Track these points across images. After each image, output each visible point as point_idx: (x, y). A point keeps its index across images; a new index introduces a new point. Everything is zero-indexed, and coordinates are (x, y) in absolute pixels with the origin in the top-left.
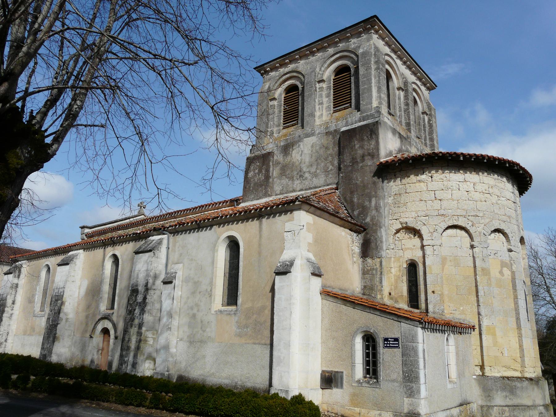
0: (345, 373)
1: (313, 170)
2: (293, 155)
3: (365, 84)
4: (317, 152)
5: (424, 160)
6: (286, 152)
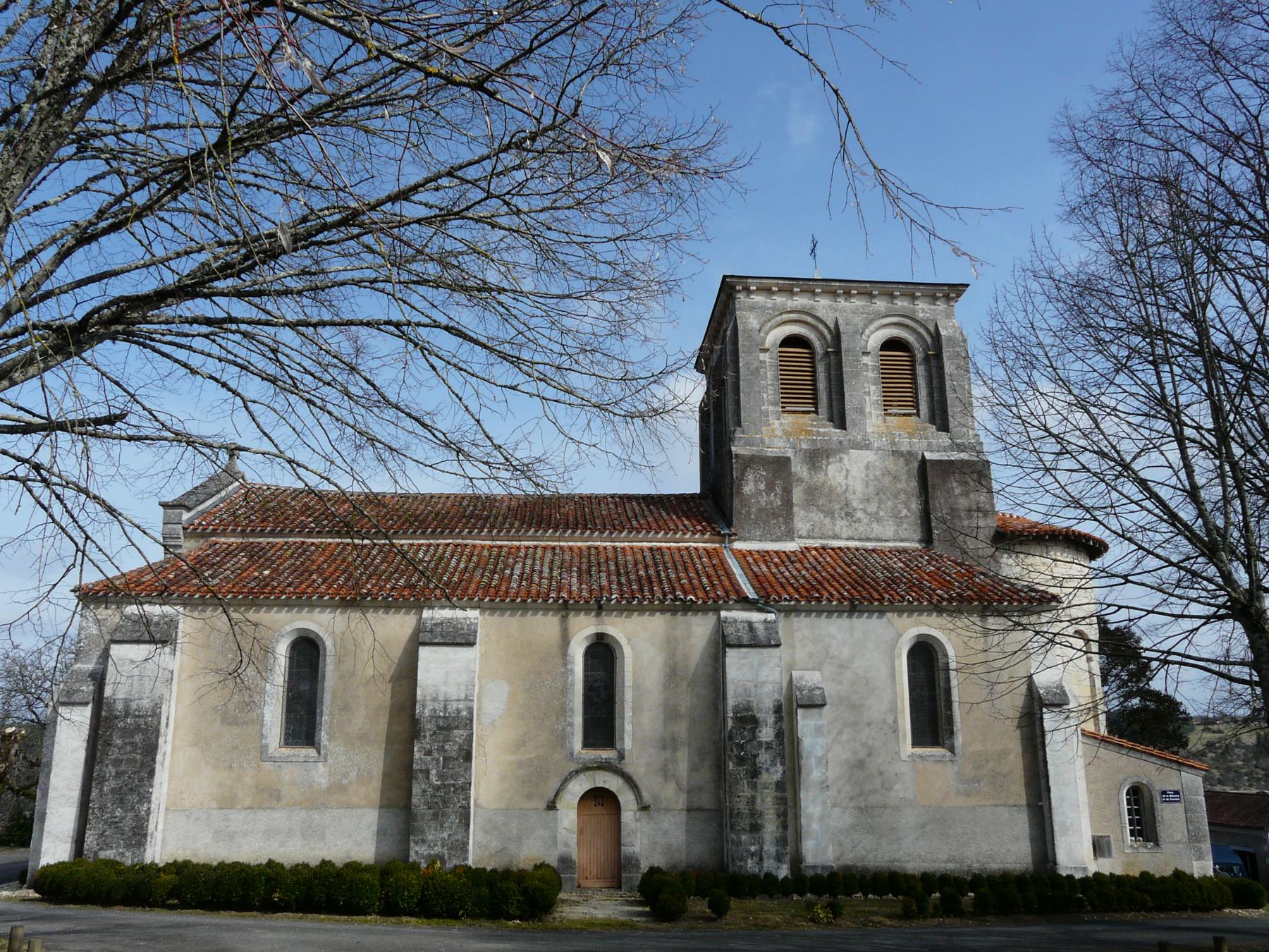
0: (1112, 837)
1: (872, 508)
2: (830, 473)
4: (877, 479)
6: (814, 464)
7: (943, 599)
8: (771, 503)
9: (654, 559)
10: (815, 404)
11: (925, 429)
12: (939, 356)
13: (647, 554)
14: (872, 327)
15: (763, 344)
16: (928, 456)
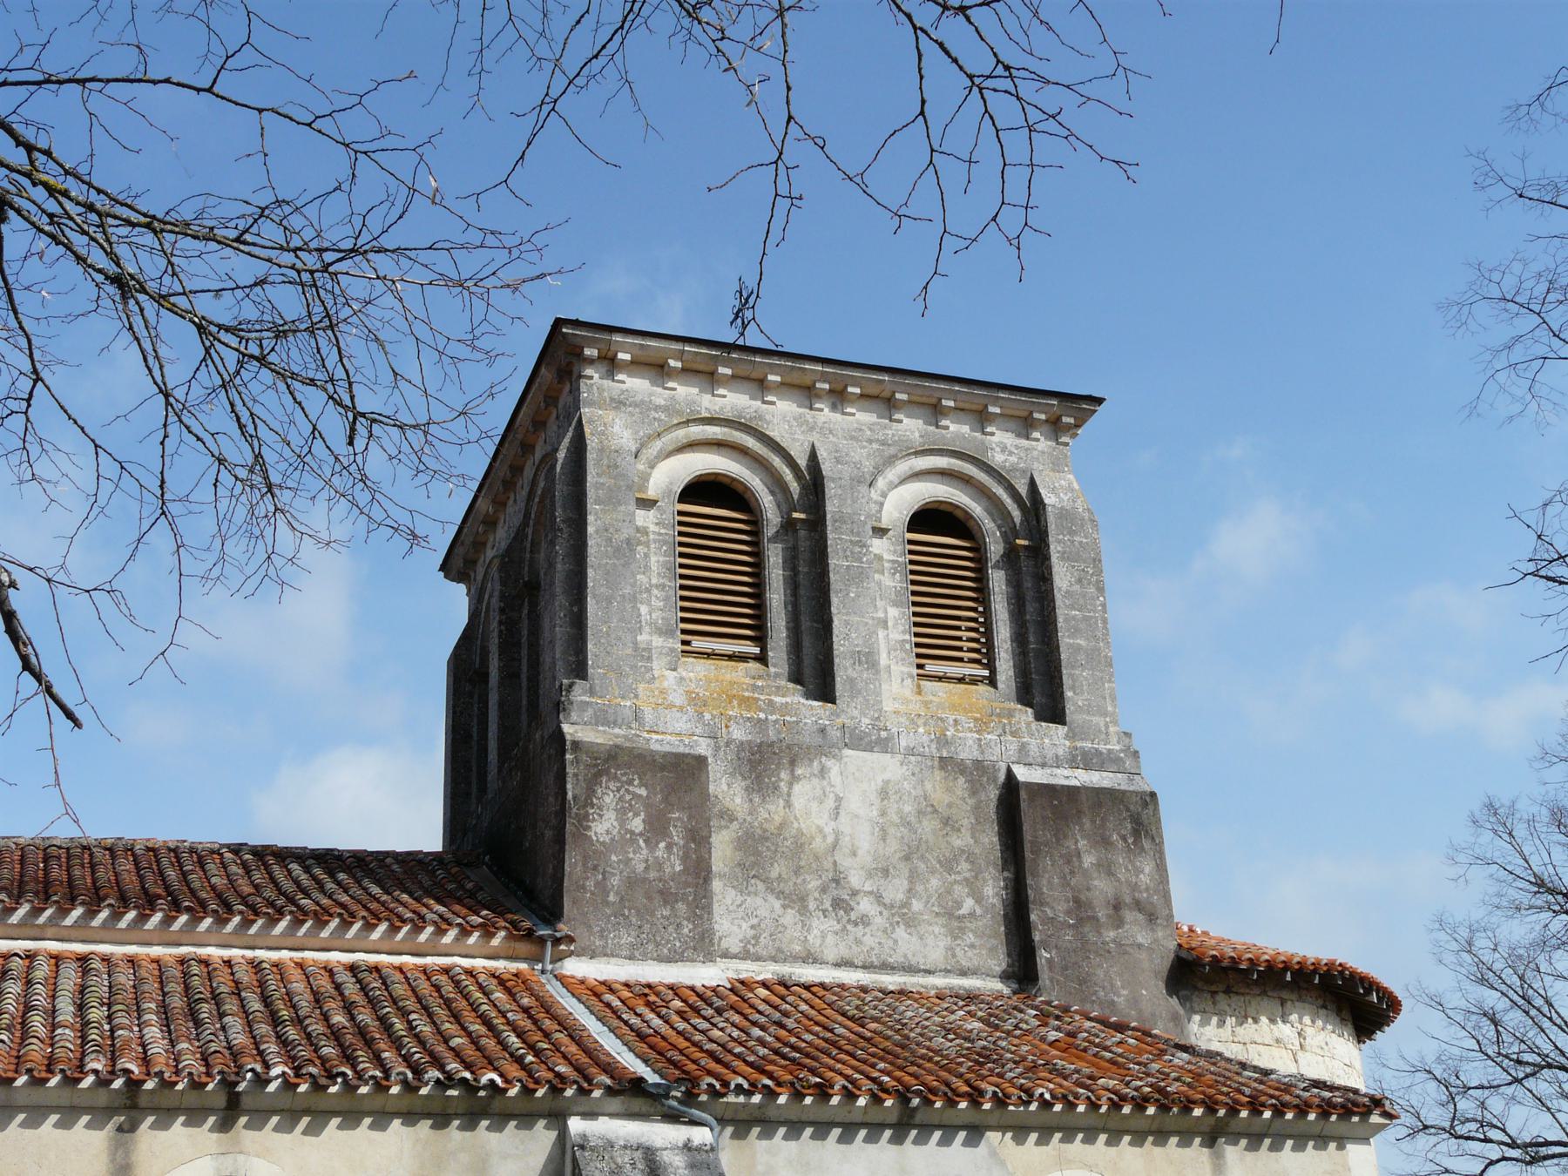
1: (895, 890)
2: (799, 802)
3: (1077, 630)
5: (1288, 978)
7: (1123, 1098)
8: (659, 865)
9: (364, 989)
10: (761, 639)
11: (1010, 714)
12: (1039, 551)
13: (344, 977)
14: (892, 474)
15: (643, 488)
16: (1022, 774)
